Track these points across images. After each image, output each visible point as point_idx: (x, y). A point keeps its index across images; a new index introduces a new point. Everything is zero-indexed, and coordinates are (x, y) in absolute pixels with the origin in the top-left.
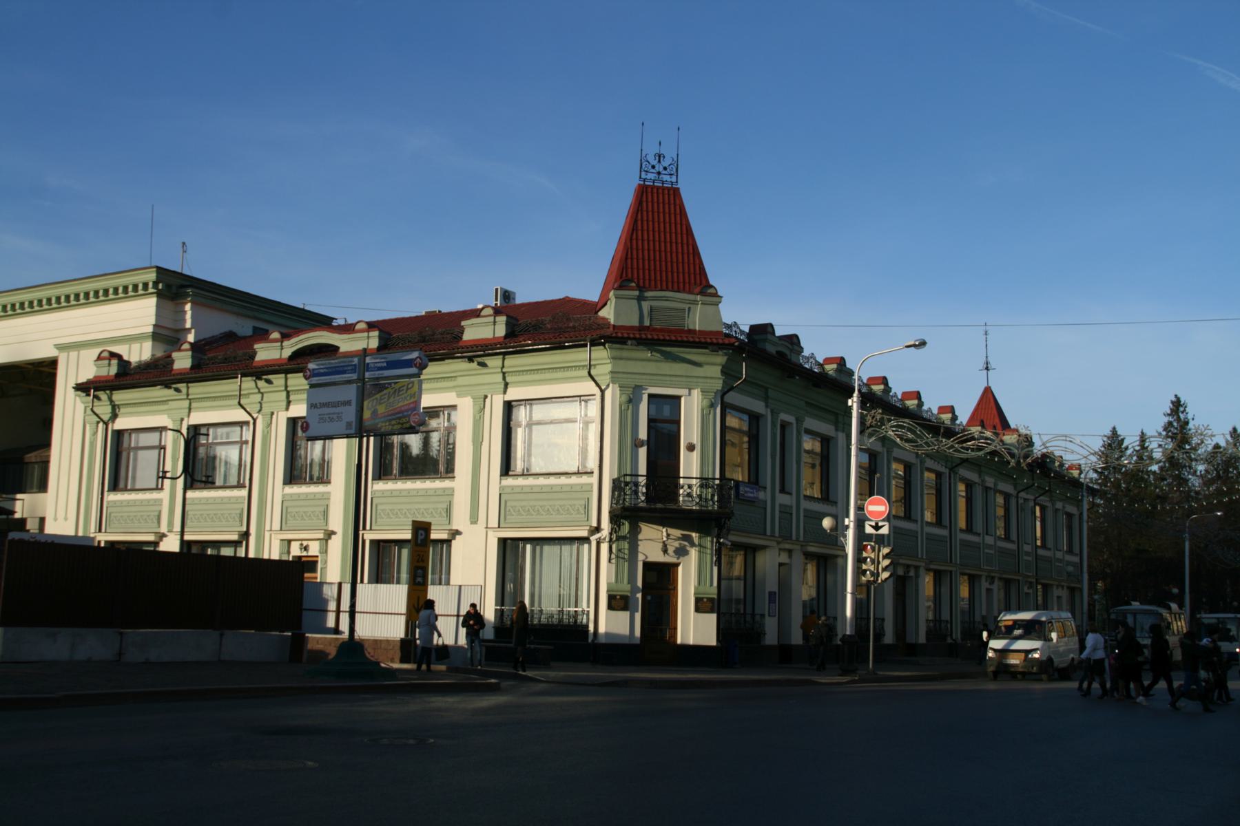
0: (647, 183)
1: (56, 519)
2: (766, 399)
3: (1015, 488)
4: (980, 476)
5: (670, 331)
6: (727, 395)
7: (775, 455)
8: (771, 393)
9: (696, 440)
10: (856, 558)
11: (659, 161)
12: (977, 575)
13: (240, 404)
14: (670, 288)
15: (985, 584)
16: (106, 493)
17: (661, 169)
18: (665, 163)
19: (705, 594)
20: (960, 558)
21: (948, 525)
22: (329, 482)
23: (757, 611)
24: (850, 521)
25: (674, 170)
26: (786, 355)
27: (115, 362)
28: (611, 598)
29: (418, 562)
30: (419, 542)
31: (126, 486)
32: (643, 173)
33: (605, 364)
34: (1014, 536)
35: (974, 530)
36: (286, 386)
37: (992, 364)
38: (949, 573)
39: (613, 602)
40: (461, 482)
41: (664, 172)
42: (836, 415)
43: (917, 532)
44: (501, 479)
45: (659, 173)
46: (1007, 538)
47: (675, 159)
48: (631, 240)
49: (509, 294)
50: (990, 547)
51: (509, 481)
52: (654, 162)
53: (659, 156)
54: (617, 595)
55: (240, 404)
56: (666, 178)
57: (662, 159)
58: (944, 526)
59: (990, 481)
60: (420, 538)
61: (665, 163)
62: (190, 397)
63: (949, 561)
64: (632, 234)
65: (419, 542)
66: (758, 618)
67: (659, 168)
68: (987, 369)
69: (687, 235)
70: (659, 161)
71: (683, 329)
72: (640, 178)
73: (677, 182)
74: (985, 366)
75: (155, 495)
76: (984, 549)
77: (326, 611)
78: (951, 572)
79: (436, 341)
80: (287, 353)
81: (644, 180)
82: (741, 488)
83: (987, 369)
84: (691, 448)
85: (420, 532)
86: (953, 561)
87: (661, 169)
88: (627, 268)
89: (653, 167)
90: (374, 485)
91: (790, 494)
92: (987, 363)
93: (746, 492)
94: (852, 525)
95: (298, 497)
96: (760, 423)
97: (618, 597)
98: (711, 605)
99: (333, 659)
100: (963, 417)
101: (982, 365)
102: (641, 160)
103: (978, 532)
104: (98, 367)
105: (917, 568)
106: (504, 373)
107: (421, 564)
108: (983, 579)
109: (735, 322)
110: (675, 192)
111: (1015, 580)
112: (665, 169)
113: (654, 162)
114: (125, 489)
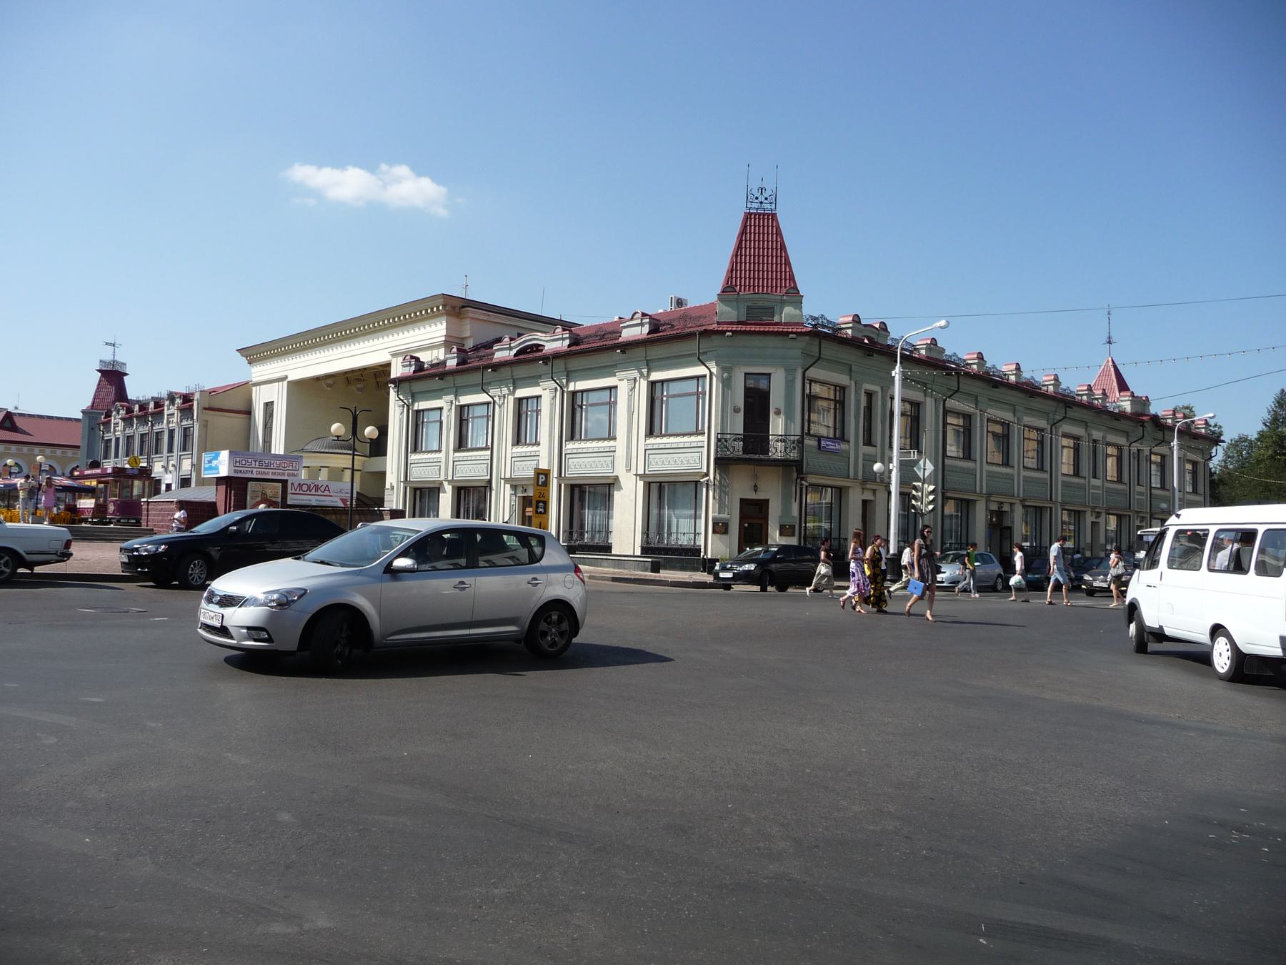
0: (751, 211)
2: (850, 372)
3: (1128, 441)
4: (1086, 429)
6: (809, 370)
7: (885, 421)
8: (853, 367)
9: (781, 405)
10: (898, 490)
12: (1082, 511)
15: (1090, 518)
16: (409, 454)
17: (763, 200)
18: (766, 195)
20: (1062, 496)
21: (1049, 470)
23: (842, 536)
24: (894, 466)
25: (774, 199)
26: (873, 339)
27: (413, 362)
28: (715, 524)
29: (539, 497)
30: (540, 483)
31: (421, 449)
34: (1126, 479)
35: (1081, 475)
36: (512, 376)
37: (1114, 339)
38: (1049, 509)
40: (620, 444)
41: (765, 201)
42: (925, 385)
43: (1013, 476)
44: (646, 440)
45: (761, 203)
46: (1120, 480)
48: (737, 256)
49: (682, 301)
50: (1096, 488)
51: (652, 441)
55: (482, 389)
57: (763, 191)
58: (1082, 477)
59: (1097, 435)
60: (541, 480)
61: (766, 195)
62: (456, 385)
63: (1049, 499)
64: (737, 252)
65: (540, 483)
66: (842, 541)
67: (762, 199)
68: (1109, 342)
69: (781, 250)
74: (1108, 340)
75: (437, 455)
76: (1089, 489)
78: (1051, 508)
82: (822, 442)
83: (1109, 342)
85: (541, 476)
86: (1054, 500)
87: (763, 200)
88: (732, 278)
89: (757, 198)
90: (567, 446)
91: (876, 446)
92: (1109, 338)
93: (828, 445)
94: (895, 469)
96: (846, 392)
99: (411, 558)
100: (1061, 387)
101: (1105, 339)
103: (1084, 476)
105: (1012, 504)
106: (647, 360)
107: (542, 499)
108: (1088, 514)
109: (823, 315)
110: (773, 216)
111: (1126, 515)
114: (421, 452)
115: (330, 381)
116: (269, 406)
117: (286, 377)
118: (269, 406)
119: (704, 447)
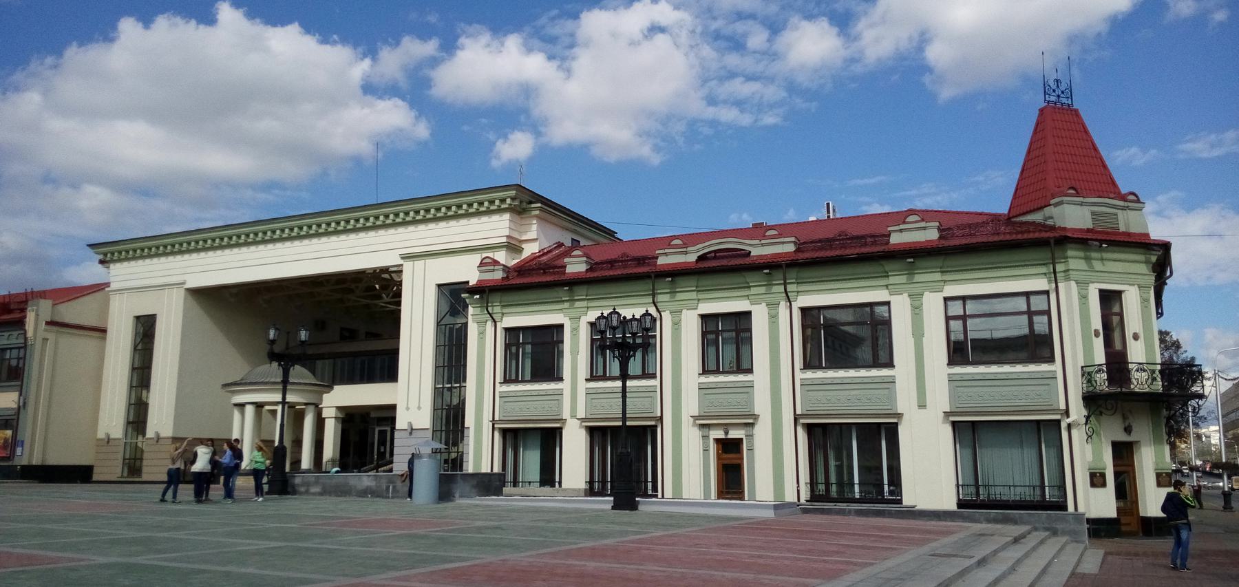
1: (408, 409)
5: (1108, 233)
11: (1058, 86)
13: (654, 302)
14: (16, 315)
19: (1096, 469)
22: (750, 371)
32: (1047, 96)
33: (55, 354)
39: (1101, 480)
41: (1062, 95)
47: (1069, 85)
52: (1054, 87)
53: (1057, 81)
54: (1097, 473)
56: (1064, 100)
61: (1063, 87)
67: (1058, 92)
70: (1058, 86)
71: (1118, 232)
72: (1045, 100)
73: (1072, 104)
77: (859, 484)
79: (812, 250)
80: (692, 258)
81: (1048, 102)
84: (1136, 337)
89: (1054, 91)
95: (515, 395)
97: (1098, 475)
98: (1169, 479)
102: (1044, 85)
104: (481, 272)
112: (1063, 92)
113: (1054, 87)
115: (234, 291)
116: (146, 328)
117: (184, 283)
118: (146, 328)
119: (500, 383)
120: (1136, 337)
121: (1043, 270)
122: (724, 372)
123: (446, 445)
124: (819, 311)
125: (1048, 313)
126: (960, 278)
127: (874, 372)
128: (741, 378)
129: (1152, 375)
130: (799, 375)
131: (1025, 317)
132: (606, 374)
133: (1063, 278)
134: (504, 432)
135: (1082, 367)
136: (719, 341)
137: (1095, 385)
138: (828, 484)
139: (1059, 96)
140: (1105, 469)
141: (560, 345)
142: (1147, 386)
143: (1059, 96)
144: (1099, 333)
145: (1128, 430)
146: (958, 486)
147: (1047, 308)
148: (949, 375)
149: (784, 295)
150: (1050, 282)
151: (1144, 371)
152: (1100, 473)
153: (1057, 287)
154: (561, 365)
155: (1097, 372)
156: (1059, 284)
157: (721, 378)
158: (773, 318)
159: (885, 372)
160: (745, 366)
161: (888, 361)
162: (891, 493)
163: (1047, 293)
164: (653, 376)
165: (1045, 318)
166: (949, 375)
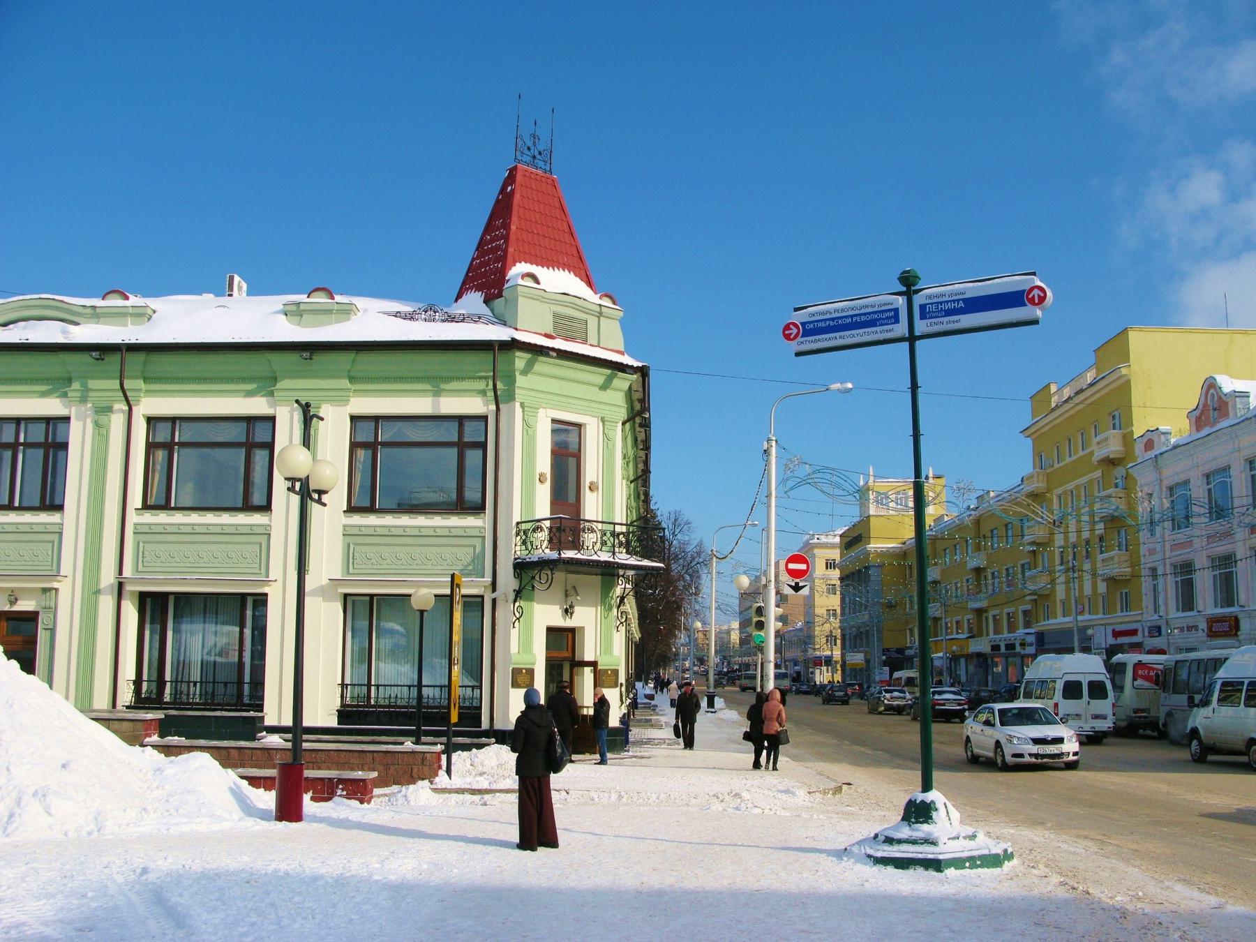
41: (538, 157)
52: (530, 144)
73: (550, 171)
97: (524, 671)
113: (530, 144)
120: (592, 488)
121: (481, 385)
122: (22, 508)
123: (969, 633)
124: (377, 423)
125: (483, 446)
126: (374, 388)
127: (242, 519)
128: (43, 517)
129: (601, 538)
130: (133, 518)
131: (454, 452)
132: (13, 503)
133: (78, 399)
134: (143, 598)
135: (518, 523)
136: (49, 462)
137: (530, 547)
138: (161, 683)
139: (534, 157)
140: (534, 664)
141: (61, 454)
142: (541, 551)
143: (534, 157)
144: (546, 479)
145: (568, 612)
146: (343, 685)
147: (270, 440)
148: (344, 526)
149: (121, 394)
150: (486, 404)
151: (592, 532)
152: (612, 670)
153: (498, 409)
154: (251, 490)
155: (534, 531)
156: (501, 406)
157: (178, 518)
158: (101, 429)
159: (257, 519)
160: (258, 498)
161: (265, 503)
162: (251, 697)
163: (484, 418)
164: (479, 509)
165: (480, 453)
166: (344, 526)
